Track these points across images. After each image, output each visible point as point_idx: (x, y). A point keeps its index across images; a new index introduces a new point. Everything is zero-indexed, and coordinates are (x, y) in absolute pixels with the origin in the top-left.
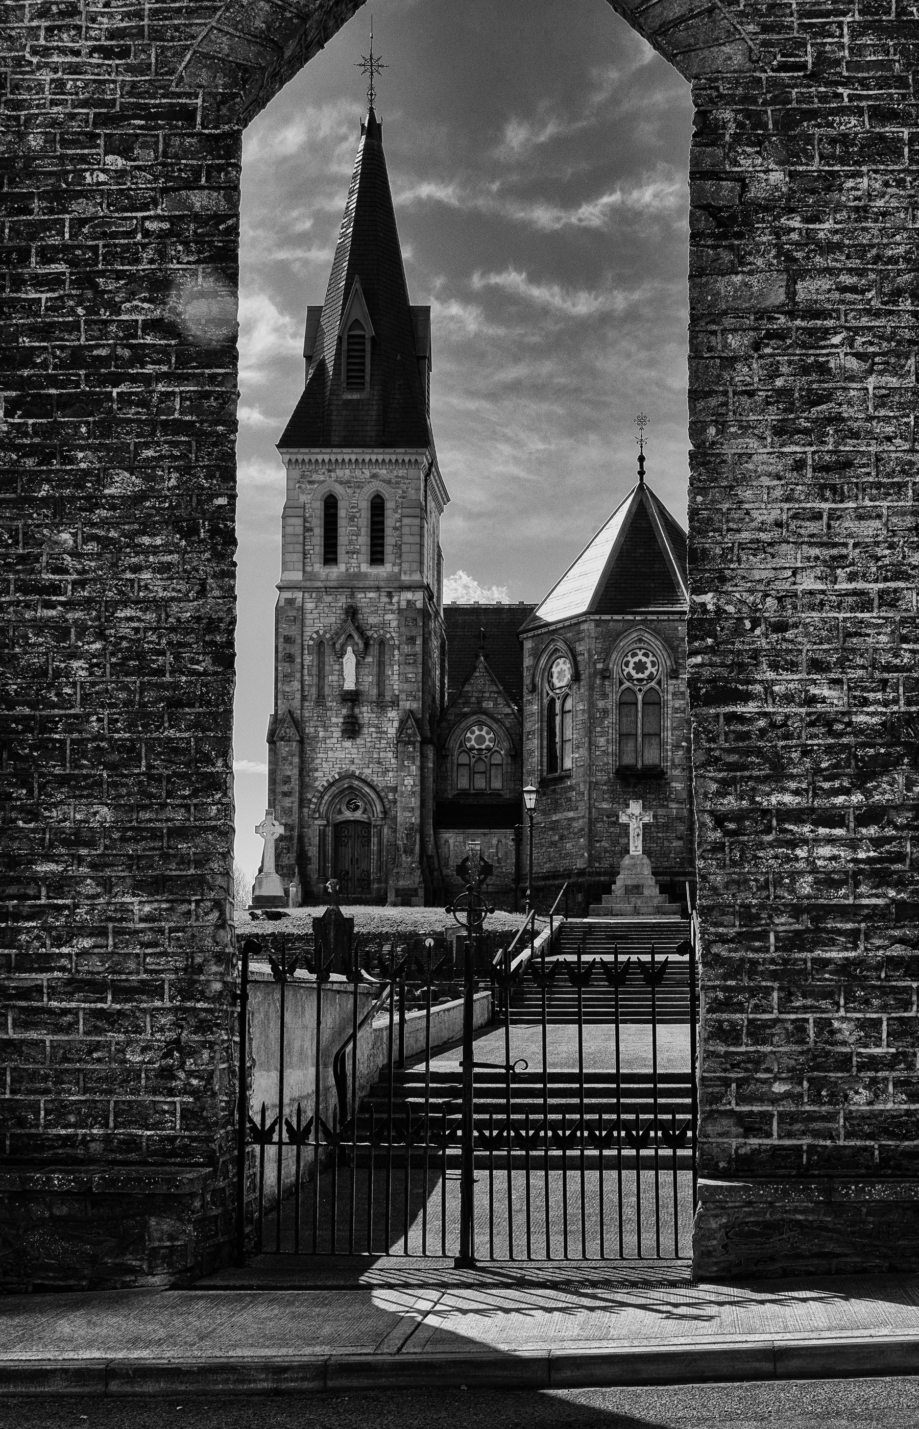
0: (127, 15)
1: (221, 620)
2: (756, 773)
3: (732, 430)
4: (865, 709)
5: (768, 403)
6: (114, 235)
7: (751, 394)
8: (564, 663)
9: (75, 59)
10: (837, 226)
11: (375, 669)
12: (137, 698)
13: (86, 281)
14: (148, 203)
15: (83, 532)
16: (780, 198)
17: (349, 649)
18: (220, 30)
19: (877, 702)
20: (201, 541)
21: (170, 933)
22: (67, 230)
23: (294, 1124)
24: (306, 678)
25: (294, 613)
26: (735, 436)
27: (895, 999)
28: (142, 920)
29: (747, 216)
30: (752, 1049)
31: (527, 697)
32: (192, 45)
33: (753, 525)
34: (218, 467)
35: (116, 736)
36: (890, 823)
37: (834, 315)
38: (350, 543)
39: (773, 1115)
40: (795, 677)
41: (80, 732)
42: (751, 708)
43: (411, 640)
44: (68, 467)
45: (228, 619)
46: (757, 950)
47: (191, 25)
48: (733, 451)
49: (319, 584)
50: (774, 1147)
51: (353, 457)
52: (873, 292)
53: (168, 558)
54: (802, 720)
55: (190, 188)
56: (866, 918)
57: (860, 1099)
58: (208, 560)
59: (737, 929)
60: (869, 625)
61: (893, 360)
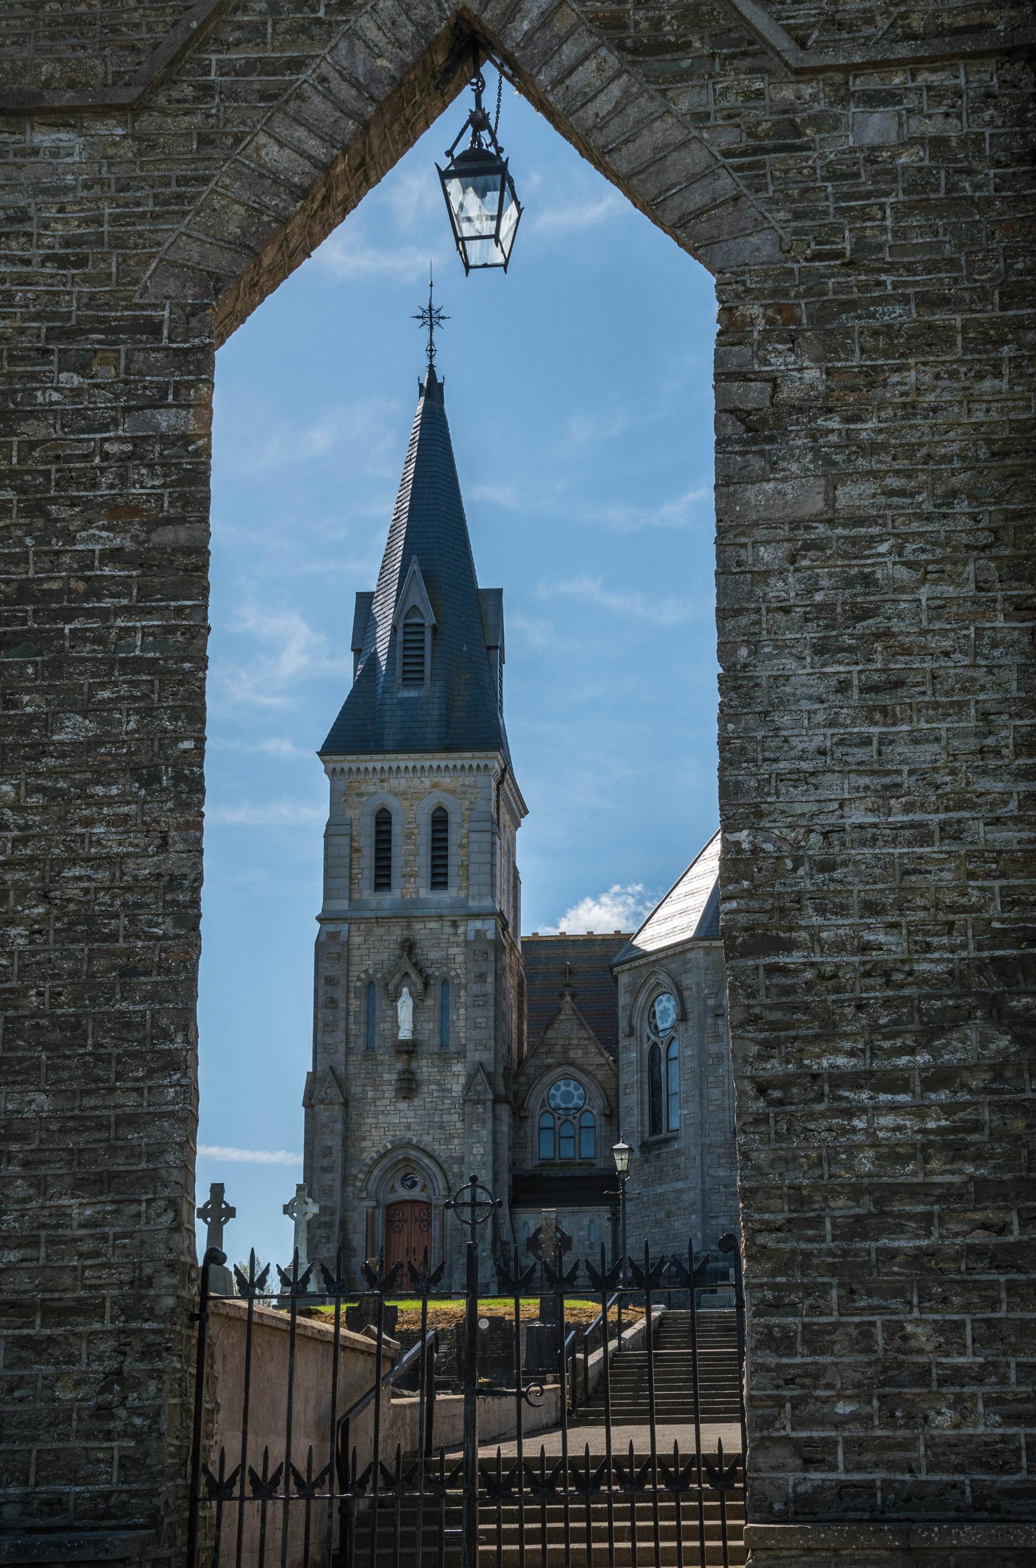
0: (86, 222)
1: (185, 876)
2: (802, 1032)
3: (767, 650)
4: (929, 956)
5: (807, 620)
6: (69, 459)
7: (786, 611)
8: (668, 1000)
9: (25, 269)
10: (882, 425)
11: (437, 1015)
12: (85, 968)
13: (36, 508)
14: (108, 424)
15: (27, 783)
16: (816, 398)
17: (405, 990)
18: (189, 236)
19: (941, 948)
20: (163, 790)
21: (115, 1239)
22: (14, 453)
23: (259, 1473)
24: (352, 1026)
25: (335, 949)
26: (770, 657)
27: (980, 1296)
28: (81, 1226)
29: (778, 418)
30: (809, 1360)
31: (623, 1042)
32: (157, 252)
33: (792, 753)
34: (183, 707)
35: (59, 1011)
36: (964, 1086)
37: (880, 521)
38: (407, 864)
39: (836, 1443)
40: (846, 922)
41: (16, 1008)
42: (796, 958)
43: (481, 977)
44: (12, 712)
45: (192, 876)
46: (811, 1240)
47: (157, 231)
48: (768, 673)
49: (369, 914)
50: (839, 1482)
51: (410, 765)
52: (924, 495)
53: (125, 809)
54: (855, 970)
55: (155, 407)
56: (941, 1199)
57: (944, 1421)
58: (171, 810)
59: (786, 1215)
60: (929, 860)
61: (948, 568)
